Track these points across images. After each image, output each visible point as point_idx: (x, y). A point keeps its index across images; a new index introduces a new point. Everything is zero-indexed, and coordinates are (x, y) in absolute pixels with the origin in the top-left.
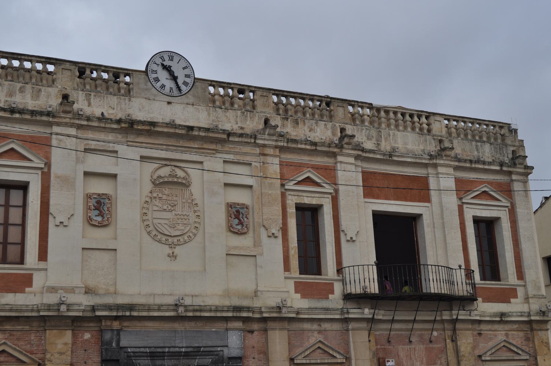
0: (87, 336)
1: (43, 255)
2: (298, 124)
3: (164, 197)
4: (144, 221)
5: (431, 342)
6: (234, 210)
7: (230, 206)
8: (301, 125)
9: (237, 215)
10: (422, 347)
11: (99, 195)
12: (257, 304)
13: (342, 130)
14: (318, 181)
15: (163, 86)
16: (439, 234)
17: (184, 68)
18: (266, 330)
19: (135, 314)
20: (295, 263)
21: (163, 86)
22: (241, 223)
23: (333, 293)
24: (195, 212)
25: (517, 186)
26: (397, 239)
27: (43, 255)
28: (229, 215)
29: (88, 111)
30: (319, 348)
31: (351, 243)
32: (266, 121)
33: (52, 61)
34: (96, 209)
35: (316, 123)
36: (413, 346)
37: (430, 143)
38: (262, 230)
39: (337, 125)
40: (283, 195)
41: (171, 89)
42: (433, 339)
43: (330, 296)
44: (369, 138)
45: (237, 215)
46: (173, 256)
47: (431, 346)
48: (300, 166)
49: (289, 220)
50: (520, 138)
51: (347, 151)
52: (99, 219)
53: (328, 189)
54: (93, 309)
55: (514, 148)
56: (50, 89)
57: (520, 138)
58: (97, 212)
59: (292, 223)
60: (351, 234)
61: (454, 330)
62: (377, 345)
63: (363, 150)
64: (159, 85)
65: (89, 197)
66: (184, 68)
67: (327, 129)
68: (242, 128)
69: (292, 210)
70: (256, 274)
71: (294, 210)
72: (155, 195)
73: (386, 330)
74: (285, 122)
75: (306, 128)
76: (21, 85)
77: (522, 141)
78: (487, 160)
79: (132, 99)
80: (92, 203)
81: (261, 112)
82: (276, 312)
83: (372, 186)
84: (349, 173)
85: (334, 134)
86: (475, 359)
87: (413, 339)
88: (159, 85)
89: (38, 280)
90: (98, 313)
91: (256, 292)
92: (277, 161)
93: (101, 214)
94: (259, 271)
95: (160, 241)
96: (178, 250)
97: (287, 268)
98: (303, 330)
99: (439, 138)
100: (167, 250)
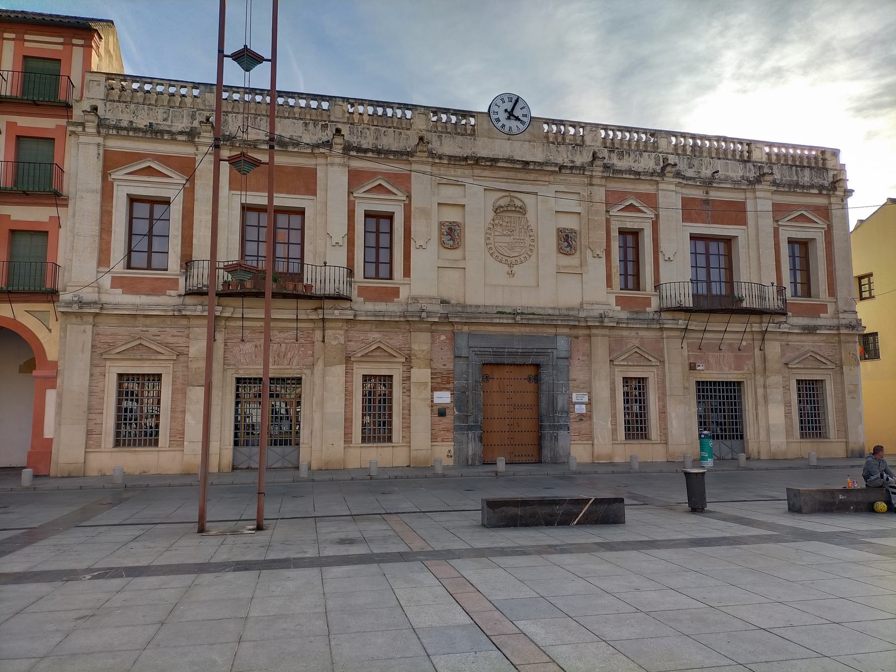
0: (443, 337)
1: (407, 273)
3: (504, 224)
6: (564, 234)
9: (567, 238)
12: (582, 314)
18: (590, 336)
20: (617, 280)
21: (503, 126)
22: (569, 245)
23: (650, 306)
27: (407, 273)
38: (589, 252)
39: (660, 155)
40: (608, 221)
45: (567, 238)
52: (451, 242)
53: (650, 214)
55: (835, 172)
58: (449, 237)
63: (684, 178)
72: (496, 222)
73: (698, 338)
80: (445, 229)
89: (404, 293)
92: (602, 191)
93: (452, 239)
95: (500, 262)
96: (515, 268)
97: (609, 284)
98: (622, 337)
100: (506, 268)
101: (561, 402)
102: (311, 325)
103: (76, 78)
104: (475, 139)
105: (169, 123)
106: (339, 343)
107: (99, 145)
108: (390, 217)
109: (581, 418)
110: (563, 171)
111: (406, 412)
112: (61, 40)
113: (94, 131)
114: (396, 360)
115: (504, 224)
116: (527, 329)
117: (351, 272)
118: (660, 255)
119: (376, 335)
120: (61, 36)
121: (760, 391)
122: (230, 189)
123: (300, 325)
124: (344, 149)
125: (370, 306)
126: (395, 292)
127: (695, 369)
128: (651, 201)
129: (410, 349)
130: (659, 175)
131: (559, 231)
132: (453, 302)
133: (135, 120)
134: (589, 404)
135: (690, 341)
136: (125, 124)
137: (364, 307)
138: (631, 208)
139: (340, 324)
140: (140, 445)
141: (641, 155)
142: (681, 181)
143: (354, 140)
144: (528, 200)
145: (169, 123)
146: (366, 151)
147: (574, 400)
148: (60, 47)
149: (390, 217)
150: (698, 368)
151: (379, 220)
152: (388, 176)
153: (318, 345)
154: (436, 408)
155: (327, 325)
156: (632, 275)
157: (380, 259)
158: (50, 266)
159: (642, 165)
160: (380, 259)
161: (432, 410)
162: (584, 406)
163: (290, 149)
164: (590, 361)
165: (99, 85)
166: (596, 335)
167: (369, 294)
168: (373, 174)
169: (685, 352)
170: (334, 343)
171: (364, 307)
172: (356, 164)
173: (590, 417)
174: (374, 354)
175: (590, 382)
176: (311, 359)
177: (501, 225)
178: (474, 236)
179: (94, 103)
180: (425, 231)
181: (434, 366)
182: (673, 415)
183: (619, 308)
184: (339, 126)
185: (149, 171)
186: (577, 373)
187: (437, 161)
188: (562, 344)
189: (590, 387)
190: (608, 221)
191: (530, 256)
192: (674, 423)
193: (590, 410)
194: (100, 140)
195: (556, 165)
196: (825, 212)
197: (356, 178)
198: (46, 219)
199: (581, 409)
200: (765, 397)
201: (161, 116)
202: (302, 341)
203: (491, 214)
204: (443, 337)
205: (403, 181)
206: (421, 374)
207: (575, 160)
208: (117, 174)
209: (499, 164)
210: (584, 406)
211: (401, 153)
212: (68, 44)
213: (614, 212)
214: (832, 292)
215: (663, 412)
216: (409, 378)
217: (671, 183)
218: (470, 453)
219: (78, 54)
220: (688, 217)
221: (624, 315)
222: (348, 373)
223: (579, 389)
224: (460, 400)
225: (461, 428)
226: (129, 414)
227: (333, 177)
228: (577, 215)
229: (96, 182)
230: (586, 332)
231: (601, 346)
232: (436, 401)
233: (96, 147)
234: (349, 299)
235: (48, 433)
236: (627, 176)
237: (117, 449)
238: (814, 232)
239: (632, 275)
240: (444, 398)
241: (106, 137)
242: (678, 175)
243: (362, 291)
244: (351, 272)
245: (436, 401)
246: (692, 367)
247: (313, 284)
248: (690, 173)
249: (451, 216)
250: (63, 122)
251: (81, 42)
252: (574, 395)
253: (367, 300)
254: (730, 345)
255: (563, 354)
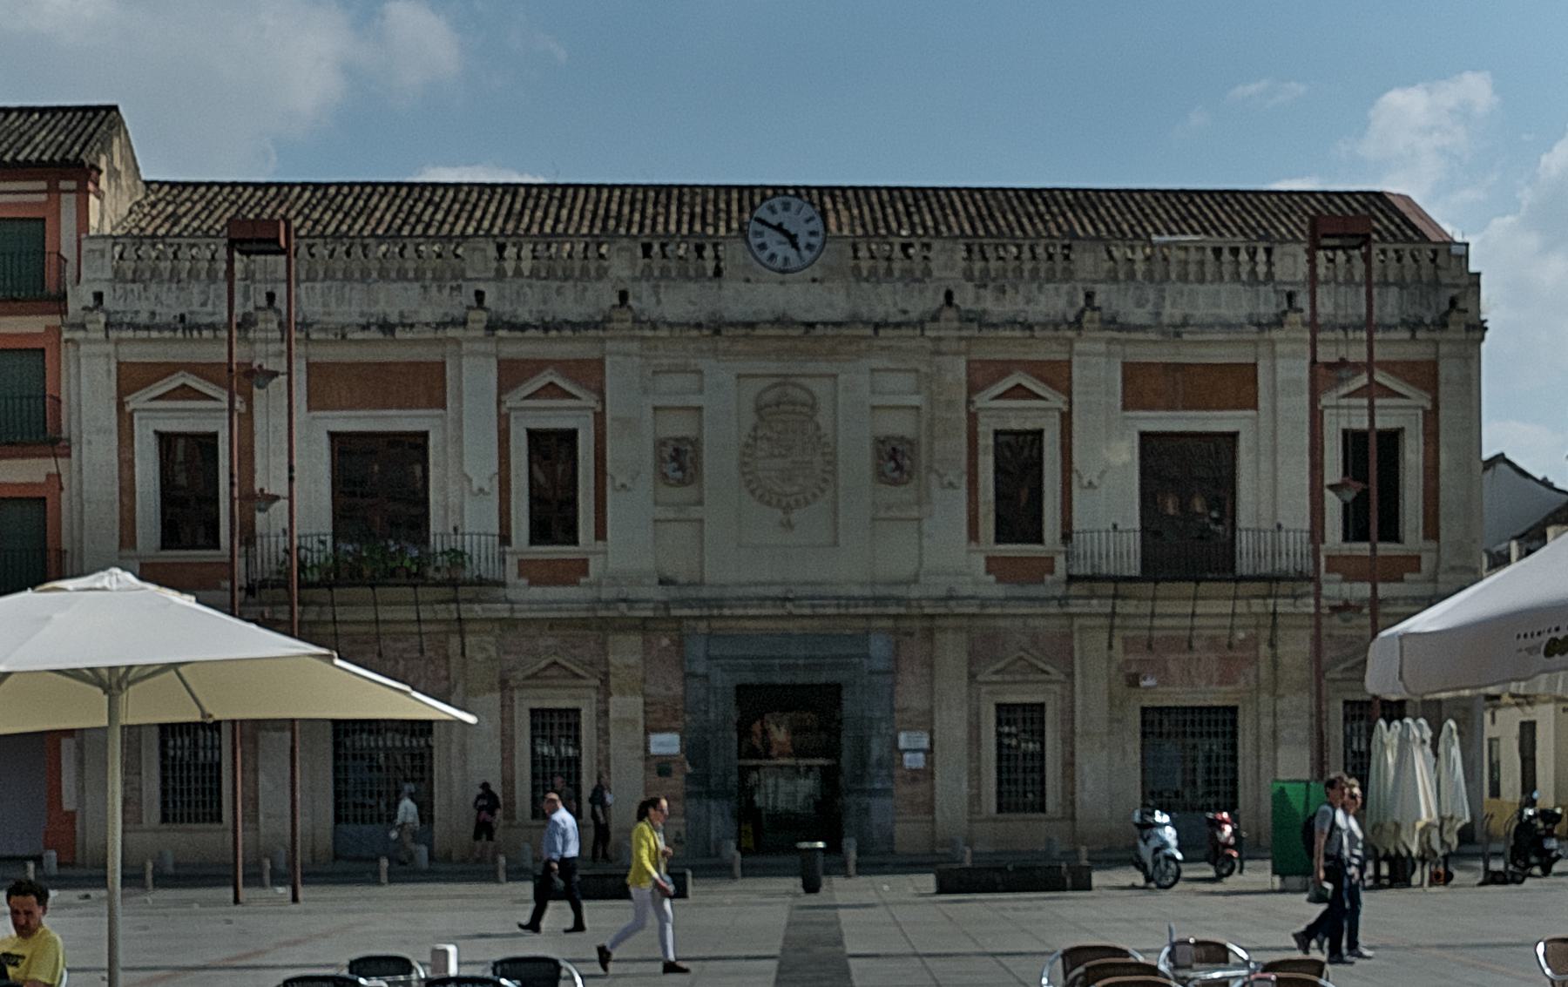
1: (601, 533)
2: (1004, 292)
4: (744, 474)
5: (1230, 646)
6: (889, 448)
7: (880, 442)
8: (1010, 292)
9: (893, 455)
10: (1213, 656)
11: (677, 440)
12: (915, 592)
13: (1089, 296)
14: (1041, 393)
15: (773, 257)
16: (1265, 466)
17: (808, 221)
19: (727, 612)
20: (988, 526)
21: (773, 257)
22: (899, 467)
23: (1052, 572)
24: (824, 454)
25: (1447, 370)
26: (1189, 489)
27: (601, 533)
28: (878, 454)
29: (653, 312)
30: (1021, 658)
31: (1090, 491)
32: (949, 296)
33: (1528, 736)
34: (674, 459)
35: (1040, 288)
36: (1196, 656)
37: (1267, 301)
38: (933, 477)
39: (1079, 286)
40: (973, 418)
41: (786, 259)
42: (1235, 642)
43: (1048, 578)
44: (1139, 305)
45: (893, 455)
46: (788, 525)
47: (1231, 654)
48: (1005, 368)
49: (981, 457)
50: (1473, 268)
51: (1092, 335)
52: (679, 474)
53: (1057, 401)
54: (666, 605)
55: (1455, 292)
56: (599, 285)
57: (1473, 268)
58: (675, 465)
59: (987, 463)
60: (1090, 475)
61: (1274, 627)
62: (1126, 651)
63: (1123, 327)
64: (767, 253)
65: (661, 443)
66: (808, 221)
67: (1058, 295)
68: (905, 312)
69: (986, 442)
70: (921, 547)
71: (991, 442)
74: (982, 291)
75: (1020, 298)
76: (558, 283)
77: (1478, 275)
78: (1388, 321)
79: (725, 285)
80: (668, 451)
81: (940, 279)
82: (587, 610)
83: (1140, 387)
84: (1097, 370)
85: (1071, 304)
86: (1117, 313)
87: (1196, 644)
88: (767, 253)
89: (594, 567)
90: (675, 612)
91: (917, 575)
92: (962, 363)
93: (681, 468)
94: (926, 542)
96: (795, 516)
97: (973, 534)
99: (1288, 288)
100: (779, 513)
101: (877, 749)
102: (443, 627)
103: (68, 252)
104: (720, 287)
105: (209, 308)
106: (489, 658)
107: (108, 356)
108: (570, 436)
109: (915, 776)
110: (882, 332)
111: (602, 768)
112: (43, 185)
113: (101, 335)
114: (584, 682)
115: (775, 436)
116: (816, 623)
117: (505, 539)
118: (1074, 476)
119: (551, 641)
120: (42, 179)
121: (1267, 722)
122: (309, 409)
123: (424, 628)
124: (487, 328)
125: (537, 592)
126: (582, 567)
127: (1137, 685)
128: (1058, 376)
129: (607, 664)
130: (1070, 325)
131: (880, 442)
132: (681, 579)
133: (158, 309)
134: (929, 752)
135: (1129, 633)
136: (143, 318)
137: (528, 597)
138: (1018, 392)
139: (489, 626)
140: (197, 821)
141: (1040, 288)
142: (1115, 334)
143: (506, 309)
144: (820, 388)
145: (209, 308)
146: (524, 327)
147: (902, 744)
148: (44, 197)
149: (570, 436)
150: (1143, 683)
151: (552, 448)
152: (563, 366)
153: (455, 661)
154: (653, 761)
155: (469, 627)
156: (1018, 512)
157: (553, 517)
158: (53, 554)
159: (1042, 307)
160: (553, 517)
161: (646, 768)
162: (921, 756)
163: (399, 334)
164: (932, 676)
165: (103, 256)
166: (944, 630)
167: (535, 573)
168: (539, 365)
169: (1118, 653)
170: (480, 657)
171: (528, 597)
172: (511, 351)
173: (932, 774)
174: (548, 673)
175: (931, 711)
176: (444, 684)
177: (769, 439)
178: (718, 461)
179: (97, 288)
180: (631, 455)
181: (651, 690)
182: (1087, 768)
183: (992, 578)
184: (481, 286)
185: (185, 392)
186: (910, 696)
187: (649, 333)
188: (879, 647)
189: (932, 720)
190: (973, 418)
191: (823, 491)
192: (1089, 785)
193: (930, 762)
194: (110, 348)
195: (866, 323)
196: (1425, 376)
197: (511, 374)
198: (41, 478)
199: (914, 761)
200: (1274, 734)
201: (197, 299)
202: (432, 654)
203: (750, 419)
204: (665, 642)
205: (590, 373)
206: (628, 706)
207: (909, 308)
208: (135, 402)
209: (759, 332)
210: (921, 756)
211: (586, 325)
212: (54, 190)
213: (982, 400)
214: (1432, 530)
215: (1069, 764)
216: (606, 712)
217: (1095, 340)
218: (713, 836)
219: (68, 203)
220: (1134, 399)
221: (1000, 591)
222: (506, 707)
223: (911, 727)
224: (695, 750)
225: (699, 795)
226: (1213, 729)
227: (474, 376)
228: (914, 412)
229: (109, 418)
230: (926, 624)
231: (952, 653)
232: (653, 750)
233: (102, 361)
234: (503, 584)
235: (68, 804)
236: (1008, 333)
237: (165, 826)
238: (1399, 414)
239: (1018, 512)
240: (667, 744)
241: (118, 342)
242: (1111, 323)
243: (525, 567)
244: (505, 539)
245: (653, 750)
246: (1133, 681)
247: (467, 549)
248: (1140, 316)
249: (678, 427)
250: (55, 320)
251: (72, 185)
252: (902, 737)
253: (533, 582)
254: (1213, 639)
255: (881, 666)
